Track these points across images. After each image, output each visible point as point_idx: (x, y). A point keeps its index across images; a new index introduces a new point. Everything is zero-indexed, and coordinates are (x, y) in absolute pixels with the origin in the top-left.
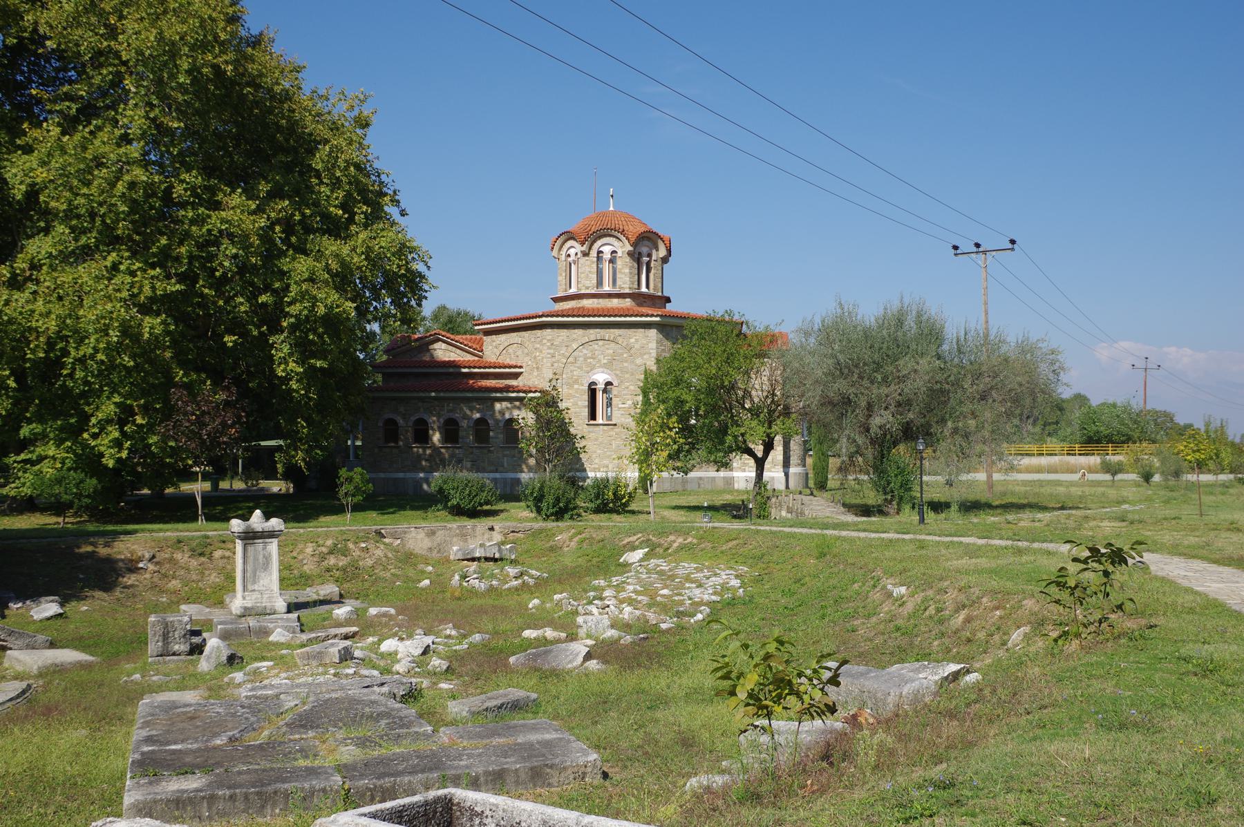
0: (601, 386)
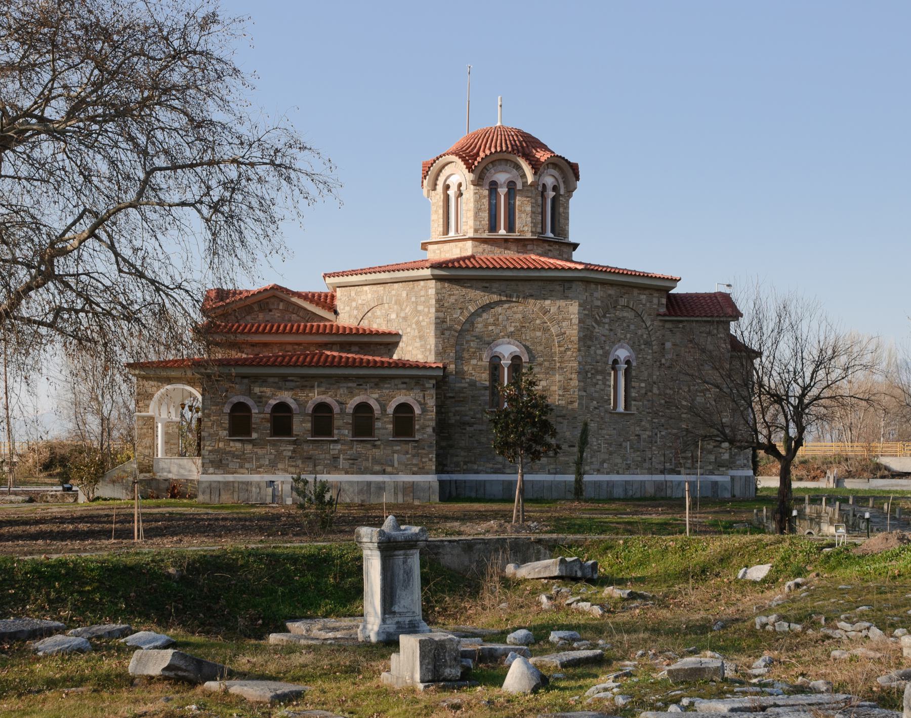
0: (506, 362)
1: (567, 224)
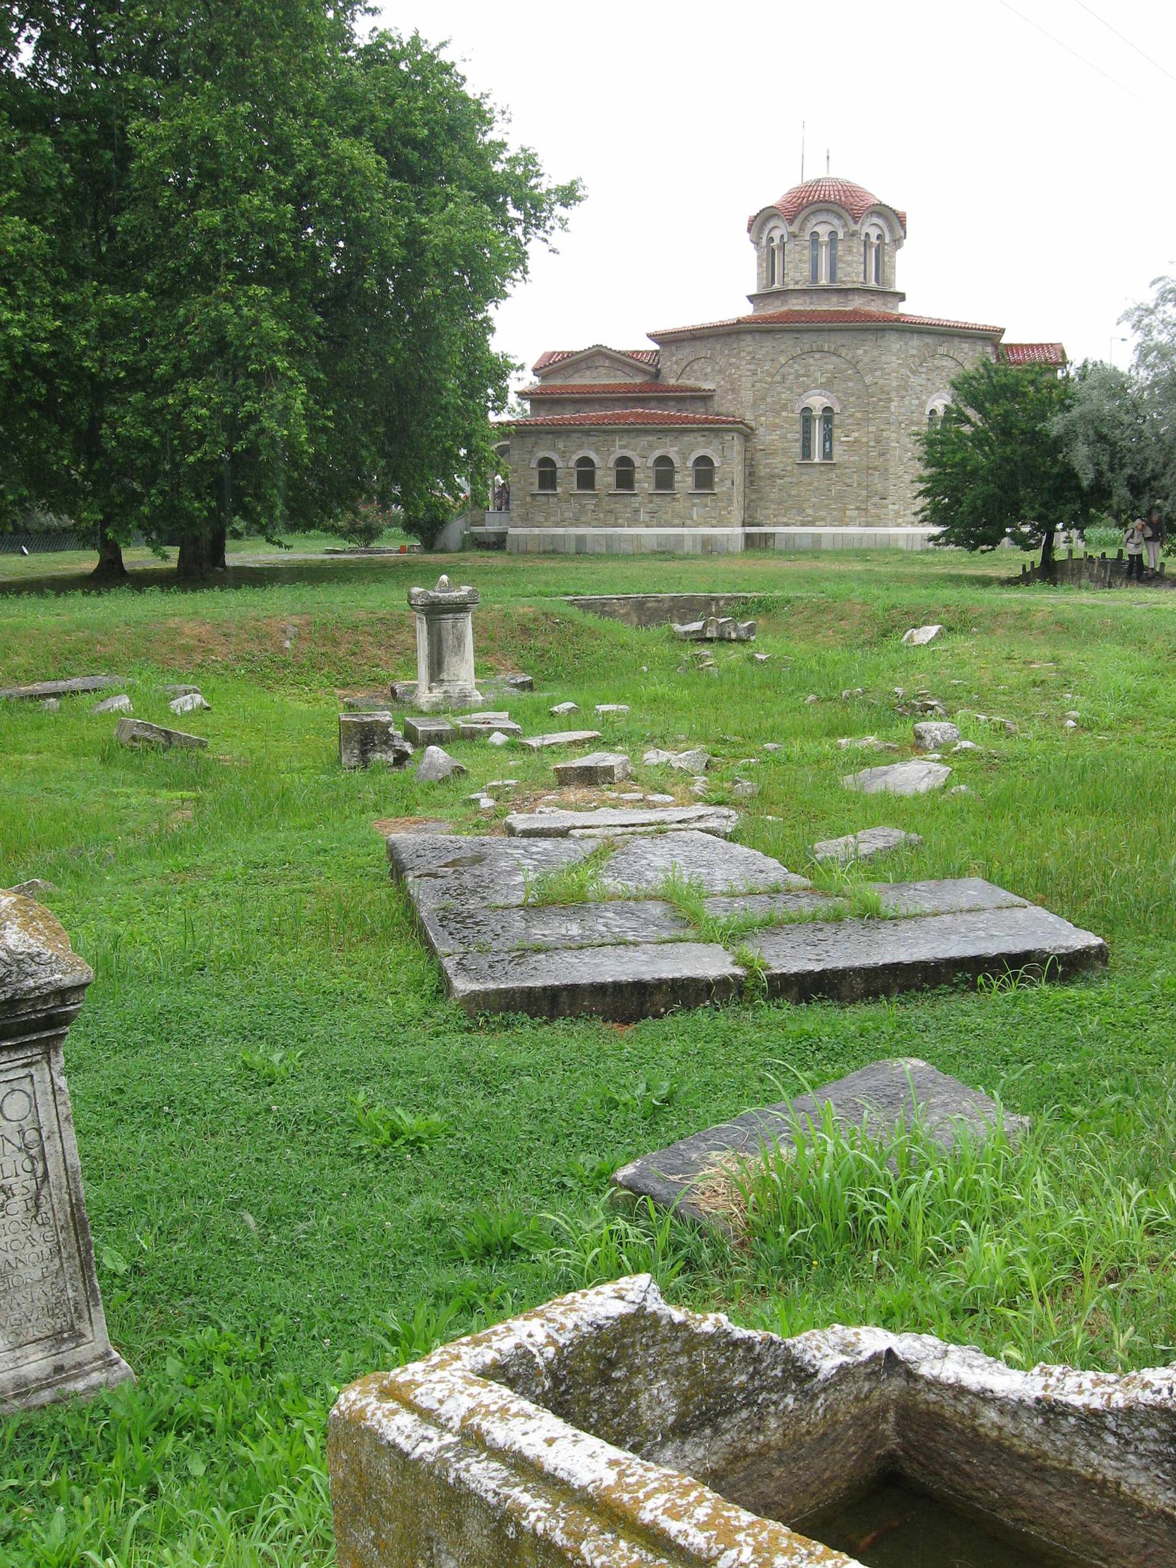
0: (818, 412)
1: (894, 273)
